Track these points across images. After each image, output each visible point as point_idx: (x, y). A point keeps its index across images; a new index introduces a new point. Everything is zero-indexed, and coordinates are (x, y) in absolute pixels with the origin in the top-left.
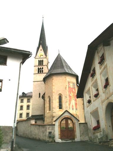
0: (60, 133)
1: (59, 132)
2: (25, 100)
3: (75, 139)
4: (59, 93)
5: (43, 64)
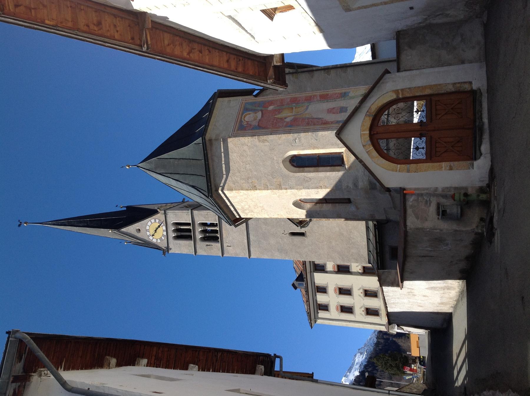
0: (443, 164)
1: (441, 168)
2: (320, 279)
3: (475, 87)
4: (18, 225)
5: (189, 224)
